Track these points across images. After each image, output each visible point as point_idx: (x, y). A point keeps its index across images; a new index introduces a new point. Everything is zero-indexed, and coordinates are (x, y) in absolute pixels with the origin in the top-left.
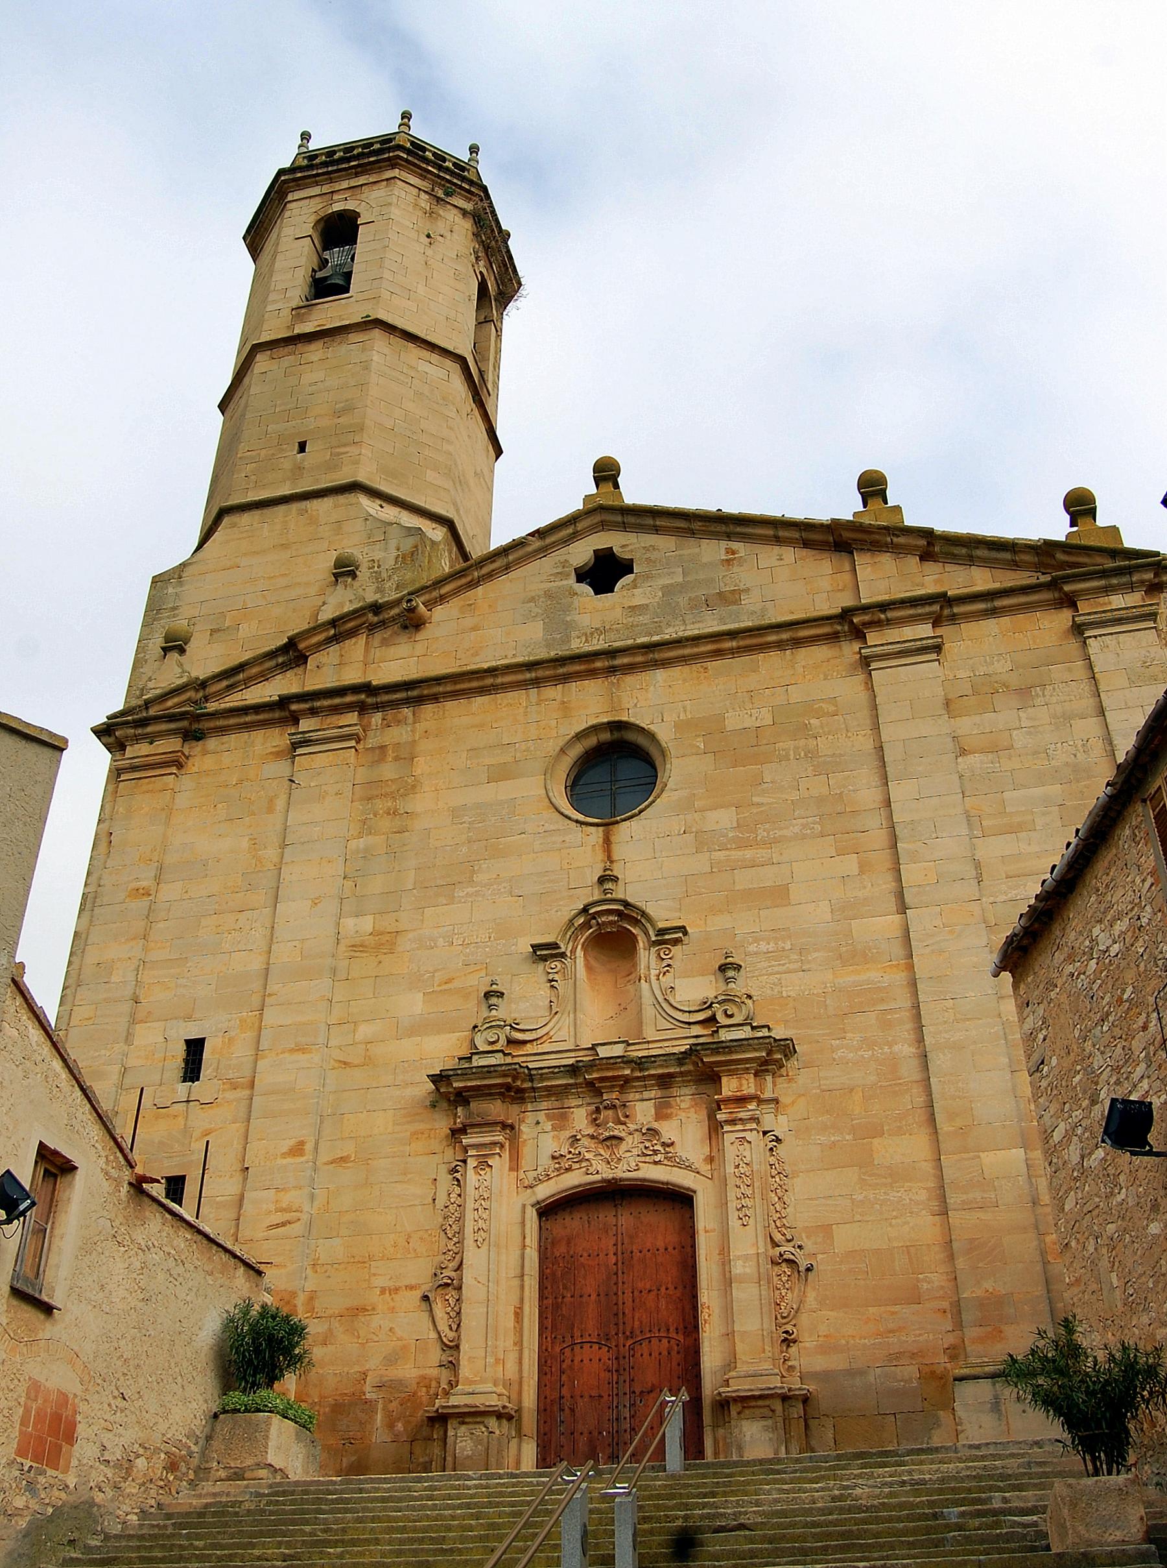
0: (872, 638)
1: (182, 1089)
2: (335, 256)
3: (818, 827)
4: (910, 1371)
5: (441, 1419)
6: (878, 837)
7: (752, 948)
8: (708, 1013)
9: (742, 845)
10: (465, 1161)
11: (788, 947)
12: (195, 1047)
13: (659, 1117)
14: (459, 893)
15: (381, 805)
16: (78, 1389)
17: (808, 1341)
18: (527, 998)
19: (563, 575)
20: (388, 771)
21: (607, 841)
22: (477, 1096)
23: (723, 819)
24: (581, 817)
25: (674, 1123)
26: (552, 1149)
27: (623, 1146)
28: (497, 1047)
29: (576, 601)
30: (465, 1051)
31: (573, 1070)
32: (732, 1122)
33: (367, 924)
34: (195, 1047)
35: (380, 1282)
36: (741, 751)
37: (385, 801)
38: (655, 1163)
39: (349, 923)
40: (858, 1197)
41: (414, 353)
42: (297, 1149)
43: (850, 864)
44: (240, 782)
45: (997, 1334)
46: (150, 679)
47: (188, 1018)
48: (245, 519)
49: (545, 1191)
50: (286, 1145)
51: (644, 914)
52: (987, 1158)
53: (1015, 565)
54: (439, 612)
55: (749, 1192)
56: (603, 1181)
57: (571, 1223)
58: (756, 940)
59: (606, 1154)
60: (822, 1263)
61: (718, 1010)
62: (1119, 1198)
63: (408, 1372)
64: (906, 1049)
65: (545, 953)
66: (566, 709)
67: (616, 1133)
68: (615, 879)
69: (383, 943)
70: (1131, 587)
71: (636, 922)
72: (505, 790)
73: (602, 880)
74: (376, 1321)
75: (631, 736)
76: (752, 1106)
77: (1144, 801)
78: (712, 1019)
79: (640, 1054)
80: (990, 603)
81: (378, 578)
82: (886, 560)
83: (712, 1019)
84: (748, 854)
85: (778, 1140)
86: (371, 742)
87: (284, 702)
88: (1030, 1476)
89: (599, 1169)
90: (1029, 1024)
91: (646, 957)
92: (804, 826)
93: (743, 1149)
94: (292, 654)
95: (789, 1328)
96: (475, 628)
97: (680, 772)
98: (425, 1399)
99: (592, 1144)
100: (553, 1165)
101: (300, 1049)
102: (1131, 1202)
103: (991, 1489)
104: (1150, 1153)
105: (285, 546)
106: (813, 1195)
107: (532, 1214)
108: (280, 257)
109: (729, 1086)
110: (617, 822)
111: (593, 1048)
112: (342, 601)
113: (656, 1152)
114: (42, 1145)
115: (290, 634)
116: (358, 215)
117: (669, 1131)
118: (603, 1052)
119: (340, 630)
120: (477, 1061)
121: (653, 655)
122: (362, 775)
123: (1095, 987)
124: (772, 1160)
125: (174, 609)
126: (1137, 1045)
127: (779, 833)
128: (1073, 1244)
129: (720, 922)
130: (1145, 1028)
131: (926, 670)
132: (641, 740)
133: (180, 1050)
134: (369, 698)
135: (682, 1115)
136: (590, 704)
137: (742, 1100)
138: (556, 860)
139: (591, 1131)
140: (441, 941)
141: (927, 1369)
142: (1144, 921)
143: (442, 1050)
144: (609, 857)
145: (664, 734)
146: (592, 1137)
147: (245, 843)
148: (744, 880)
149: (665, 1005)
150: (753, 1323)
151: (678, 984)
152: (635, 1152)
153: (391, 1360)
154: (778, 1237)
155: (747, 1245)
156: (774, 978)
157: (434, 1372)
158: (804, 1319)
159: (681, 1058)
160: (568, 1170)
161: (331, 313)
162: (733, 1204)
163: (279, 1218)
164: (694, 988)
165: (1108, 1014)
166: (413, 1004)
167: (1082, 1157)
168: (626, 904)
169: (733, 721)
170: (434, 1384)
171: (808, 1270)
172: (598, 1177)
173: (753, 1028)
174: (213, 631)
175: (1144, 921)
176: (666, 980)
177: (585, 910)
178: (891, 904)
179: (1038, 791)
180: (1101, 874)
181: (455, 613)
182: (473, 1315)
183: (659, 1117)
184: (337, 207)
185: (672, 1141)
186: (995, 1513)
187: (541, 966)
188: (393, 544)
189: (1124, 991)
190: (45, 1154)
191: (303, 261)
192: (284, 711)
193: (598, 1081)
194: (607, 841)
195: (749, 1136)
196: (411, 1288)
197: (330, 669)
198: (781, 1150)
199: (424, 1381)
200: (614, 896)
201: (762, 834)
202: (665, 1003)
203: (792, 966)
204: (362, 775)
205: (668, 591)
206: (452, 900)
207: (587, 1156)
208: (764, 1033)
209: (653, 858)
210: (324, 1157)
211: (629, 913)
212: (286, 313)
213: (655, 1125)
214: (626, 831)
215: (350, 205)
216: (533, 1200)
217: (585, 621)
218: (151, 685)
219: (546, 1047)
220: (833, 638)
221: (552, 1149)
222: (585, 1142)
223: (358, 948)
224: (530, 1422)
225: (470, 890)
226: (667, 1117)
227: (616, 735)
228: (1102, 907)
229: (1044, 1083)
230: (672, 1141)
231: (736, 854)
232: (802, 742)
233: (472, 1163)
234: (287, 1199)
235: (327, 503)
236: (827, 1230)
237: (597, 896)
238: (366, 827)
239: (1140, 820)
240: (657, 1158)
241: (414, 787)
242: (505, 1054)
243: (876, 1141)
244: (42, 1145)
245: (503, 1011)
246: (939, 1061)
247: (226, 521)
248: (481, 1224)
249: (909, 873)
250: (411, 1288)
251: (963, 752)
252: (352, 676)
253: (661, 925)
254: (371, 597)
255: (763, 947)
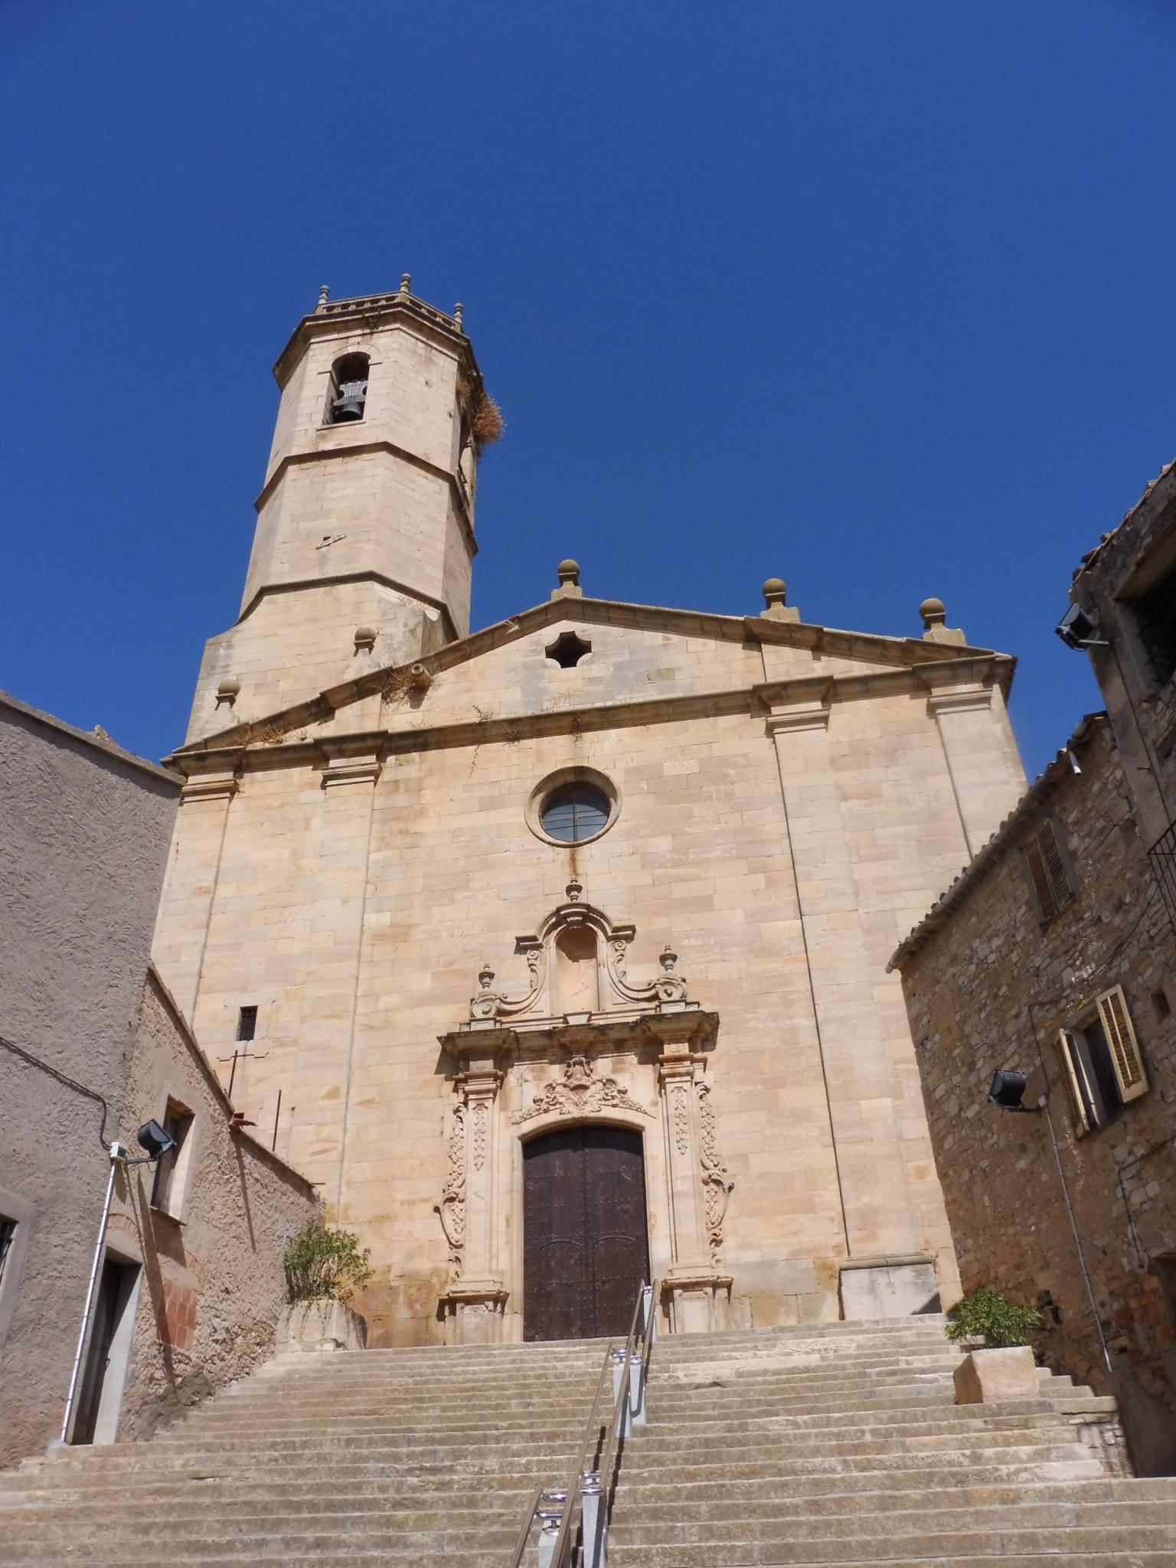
0: (775, 710)
1: (240, 1045)
2: (350, 389)
3: (734, 852)
4: (807, 1263)
5: (449, 1305)
6: (782, 859)
7: (686, 943)
8: (653, 992)
9: (676, 864)
10: (466, 1104)
11: (712, 942)
12: (249, 1015)
13: (615, 1071)
14: (458, 896)
15: (395, 826)
16: (197, 1286)
17: (729, 1242)
18: (514, 978)
19: (535, 652)
20: (401, 800)
21: (573, 860)
22: (473, 1056)
23: (662, 845)
24: (552, 840)
25: (628, 1075)
26: (533, 1094)
27: (589, 1092)
28: (491, 1015)
29: (547, 672)
30: (467, 1019)
31: (549, 1034)
32: (673, 1075)
33: (386, 919)
34: (249, 1015)
35: (400, 1196)
36: (674, 792)
37: (398, 825)
38: (614, 1106)
39: (371, 918)
40: (768, 1132)
41: (414, 470)
42: (333, 1094)
43: (760, 880)
44: (282, 806)
45: (872, 1236)
46: (207, 722)
47: (244, 990)
48: (281, 597)
49: (528, 1127)
50: (325, 1090)
51: (602, 915)
52: (865, 1104)
53: (882, 660)
54: (441, 676)
55: (685, 1128)
56: (574, 1119)
57: (557, 1161)
58: (689, 937)
59: (575, 1098)
60: (740, 1183)
61: (660, 989)
62: (991, 1141)
63: (423, 1265)
64: (805, 1023)
65: (525, 945)
66: (540, 757)
67: (583, 1082)
68: (579, 889)
69: (398, 934)
70: (972, 680)
71: (596, 922)
72: (494, 817)
73: (569, 889)
74: (398, 1226)
75: (591, 779)
76: (688, 1063)
77: (1021, 849)
78: (655, 997)
79: (602, 1022)
80: (864, 687)
81: (390, 649)
82: (787, 652)
83: (655, 997)
84: (682, 871)
85: (707, 1090)
86: (385, 776)
87: (319, 743)
88: (920, 1343)
89: (571, 1109)
90: (915, 1010)
91: (604, 947)
92: (724, 851)
93: (683, 1096)
94: (323, 707)
95: (716, 1231)
96: (468, 691)
97: (625, 807)
98: (437, 1286)
99: (565, 1091)
100: (535, 1106)
101: (335, 1016)
102: (1002, 1144)
103: (897, 1353)
104: (1023, 1110)
105: (314, 620)
106: (733, 1132)
107: (518, 1145)
108: (306, 388)
109: (670, 1050)
110: (581, 845)
111: (565, 1017)
112: (363, 666)
113: (613, 1097)
114: (170, 1099)
115: (323, 690)
116: (367, 357)
117: (623, 1081)
118: (572, 1021)
119: (360, 689)
120: (476, 1027)
121: (609, 717)
122: (379, 802)
123: (974, 985)
124: (702, 1104)
125: (227, 666)
126: (1011, 1028)
127: (705, 856)
128: (951, 1173)
129: (659, 924)
130: (1017, 1016)
131: (814, 735)
132: (598, 782)
133: (236, 1015)
134: (384, 744)
135: (633, 1069)
136: (557, 753)
137: (680, 1059)
138: (531, 873)
139: (563, 1080)
140: (444, 934)
141: (820, 1262)
142: (1019, 939)
143: (449, 1018)
144: (575, 871)
145: (616, 777)
146: (565, 1086)
147: (286, 854)
148: (679, 891)
149: (620, 986)
150: (692, 1228)
151: (629, 969)
152: (598, 1097)
153: (410, 1256)
154: (707, 1163)
155: (687, 1169)
156: (702, 966)
157: (444, 1265)
158: (726, 1224)
159: (633, 1026)
160: (546, 1111)
161: (346, 435)
162: (674, 1138)
163: (318, 1147)
164: (643, 973)
165: (985, 1005)
166: (424, 982)
167: (961, 1109)
168: (588, 907)
169: (671, 768)
170: (443, 1275)
171: (731, 1188)
172: (569, 1116)
173: (687, 1004)
174: (257, 685)
175: (1019, 939)
176: (621, 966)
177: (559, 910)
178: (792, 911)
179: (900, 829)
180: (980, 901)
181: (452, 678)
182: (477, 1224)
183: (615, 1071)
184: (351, 349)
185: (627, 1089)
186: (904, 1372)
187: (524, 957)
188: (401, 621)
189: (999, 988)
190: (173, 1105)
191: (324, 392)
192: (316, 754)
193: (571, 1045)
194: (573, 860)
195: (686, 1086)
196: (425, 1200)
197: (351, 720)
198: (709, 1096)
199: (435, 1272)
200: (579, 901)
201: (692, 856)
202: (620, 983)
203: (716, 957)
204: (379, 802)
205: (618, 667)
206: (452, 901)
207: (561, 1100)
208: (694, 1008)
209: (609, 870)
210: (352, 1101)
211: (591, 915)
212: (312, 434)
213: (613, 1077)
214: (584, 852)
215: (363, 349)
216: (519, 1133)
217: (554, 688)
218: (208, 726)
219: (528, 1016)
220: (744, 709)
221: (533, 1094)
222: (559, 1089)
223: (380, 937)
224: (516, 1300)
225: (467, 894)
226: (620, 1071)
227: (579, 778)
228: (982, 927)
229: (928, 1055)
230: (627, 1089)
231: (673, 871)
232: (722, 787)
233: (472, 1104)
234: (326, 1132)
235: (348, 587)
236: (743, 1158)
237: (566, 900)
238: (384, 844)
239: (1015, 860)
240: (615, 1102)
241: (421, 813)
242: (496, 1021)
243: (781, 1091)
244: (170, 1099)
245: (495, 988)
246: (827, 1032)
247: (266, 598)
248: (480, 1151)
249: (807, 889)
250: (425, 1200)
251: (845, 798)
252: (370, 726)
253: (616, 924)
254: (385, 663)
255: (694, 942)
